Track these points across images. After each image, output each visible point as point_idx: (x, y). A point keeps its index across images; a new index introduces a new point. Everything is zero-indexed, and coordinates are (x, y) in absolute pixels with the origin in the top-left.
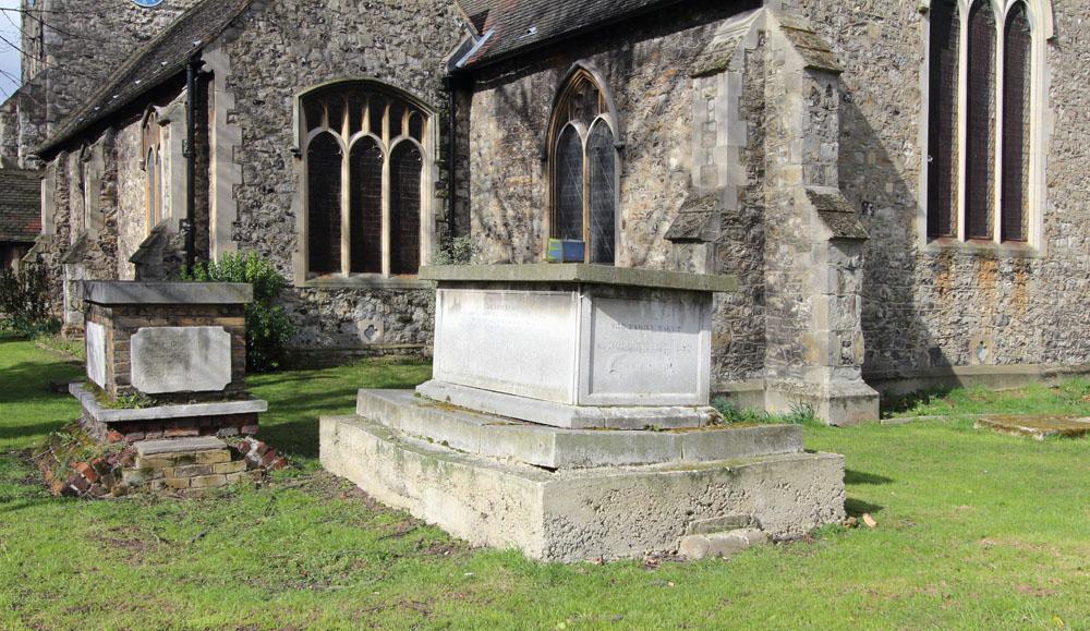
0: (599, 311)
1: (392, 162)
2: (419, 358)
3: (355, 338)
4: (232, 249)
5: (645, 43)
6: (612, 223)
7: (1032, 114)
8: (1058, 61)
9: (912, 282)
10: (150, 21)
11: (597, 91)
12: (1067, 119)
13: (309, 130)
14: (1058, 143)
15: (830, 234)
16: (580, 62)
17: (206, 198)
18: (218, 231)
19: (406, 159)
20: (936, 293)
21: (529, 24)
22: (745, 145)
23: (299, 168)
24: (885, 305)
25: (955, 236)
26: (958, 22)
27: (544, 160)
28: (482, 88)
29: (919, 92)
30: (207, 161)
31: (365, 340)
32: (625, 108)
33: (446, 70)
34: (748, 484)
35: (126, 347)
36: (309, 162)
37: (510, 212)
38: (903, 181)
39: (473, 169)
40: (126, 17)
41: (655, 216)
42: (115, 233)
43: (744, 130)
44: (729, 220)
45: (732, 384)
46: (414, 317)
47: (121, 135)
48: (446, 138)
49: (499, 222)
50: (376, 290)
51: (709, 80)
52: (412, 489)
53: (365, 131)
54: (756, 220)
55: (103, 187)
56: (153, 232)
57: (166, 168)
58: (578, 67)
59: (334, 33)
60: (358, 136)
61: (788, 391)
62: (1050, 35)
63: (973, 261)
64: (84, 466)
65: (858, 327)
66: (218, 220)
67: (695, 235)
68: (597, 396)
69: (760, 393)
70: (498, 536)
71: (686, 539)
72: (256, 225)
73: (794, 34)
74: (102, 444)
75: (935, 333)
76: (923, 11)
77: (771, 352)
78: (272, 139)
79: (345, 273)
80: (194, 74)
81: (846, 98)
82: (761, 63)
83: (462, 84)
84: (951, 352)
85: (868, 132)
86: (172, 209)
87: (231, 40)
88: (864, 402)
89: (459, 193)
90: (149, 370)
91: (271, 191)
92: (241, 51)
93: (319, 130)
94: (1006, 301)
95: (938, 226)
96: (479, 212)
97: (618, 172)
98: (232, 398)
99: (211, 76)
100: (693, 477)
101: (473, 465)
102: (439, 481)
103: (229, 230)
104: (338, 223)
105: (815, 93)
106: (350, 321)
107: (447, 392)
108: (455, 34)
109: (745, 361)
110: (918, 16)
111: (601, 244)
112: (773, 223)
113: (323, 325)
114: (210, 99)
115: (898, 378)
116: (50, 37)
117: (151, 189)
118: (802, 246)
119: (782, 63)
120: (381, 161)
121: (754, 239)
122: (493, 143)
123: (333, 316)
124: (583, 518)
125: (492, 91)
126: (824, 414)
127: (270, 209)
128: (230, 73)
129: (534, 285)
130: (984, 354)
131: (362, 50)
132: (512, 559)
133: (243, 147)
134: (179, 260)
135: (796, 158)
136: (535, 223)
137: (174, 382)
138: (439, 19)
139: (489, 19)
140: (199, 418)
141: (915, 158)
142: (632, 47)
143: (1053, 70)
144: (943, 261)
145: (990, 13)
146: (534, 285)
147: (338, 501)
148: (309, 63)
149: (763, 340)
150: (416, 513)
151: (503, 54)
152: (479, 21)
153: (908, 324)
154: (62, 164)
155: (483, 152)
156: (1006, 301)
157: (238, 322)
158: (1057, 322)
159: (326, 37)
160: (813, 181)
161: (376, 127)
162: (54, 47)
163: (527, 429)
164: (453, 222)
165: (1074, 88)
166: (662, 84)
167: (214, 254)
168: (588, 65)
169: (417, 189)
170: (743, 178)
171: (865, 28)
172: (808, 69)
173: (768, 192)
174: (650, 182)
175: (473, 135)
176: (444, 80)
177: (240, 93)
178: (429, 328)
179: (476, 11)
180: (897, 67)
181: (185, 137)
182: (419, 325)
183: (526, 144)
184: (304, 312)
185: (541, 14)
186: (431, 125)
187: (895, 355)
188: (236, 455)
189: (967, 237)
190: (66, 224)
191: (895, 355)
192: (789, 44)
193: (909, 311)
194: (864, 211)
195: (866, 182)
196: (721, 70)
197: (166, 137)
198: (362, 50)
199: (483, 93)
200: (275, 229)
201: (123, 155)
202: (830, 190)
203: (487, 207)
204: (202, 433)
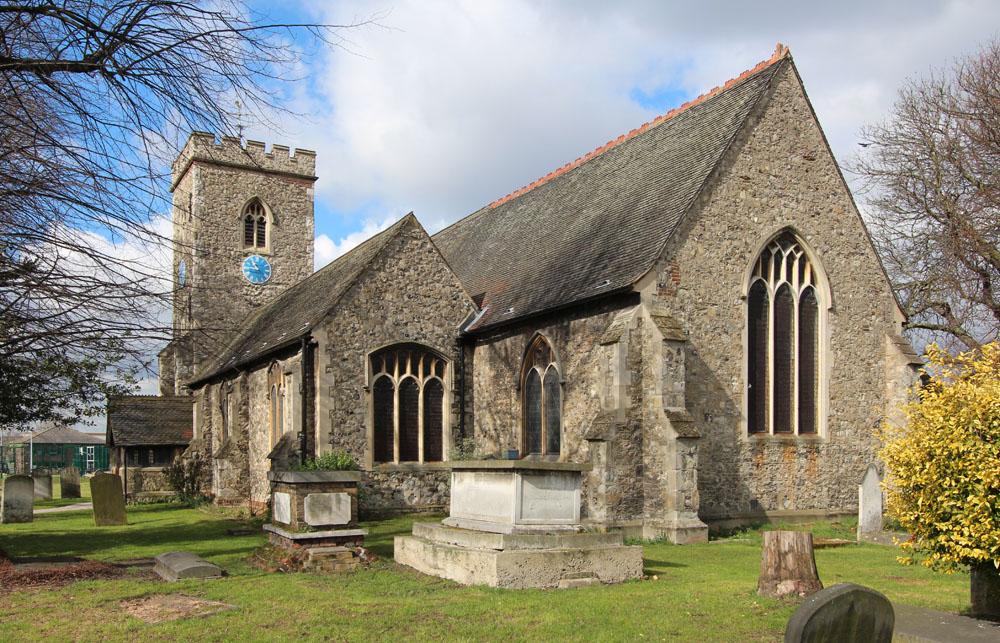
0: (525, 482)
1: (425, 392)
2: (440, 512)
3: (402, 502)
4: (329, 449)
5: (576, 321)
6: (559, 428)
7: (820, 356)
8: (836, 321)
9: (738, 461)
10: (260, 293)
11: (550, 348)
12: (843, 357)
13: (374, 374)
14: (837, 373)
15: (677, 435)
16: (539, 331)
17: (313, 418)
18: (321, 437)
19: (434, 390)
20: (755, 468)
21: (510, 305)
22: (630, 383)
23: (369, 398)
24: (721, 474)
25: (768, 432)
26: (768, 302)
27: (518, 390)
28: (481, 344)
29: (741, 347)
30: (314, 396)
31: (409, 503)
32: (565, 359)
33: (458, 333)
34: (591, 558)
35: (302, 503)
36: (374, 394)
37: (498, 422)
38: (731, 400)
39: (475, 395)
40: (245, 292)
41: (583, 424)
42: (247, 438)
43: (630, 376)
44: (620, 428)
45: (623, 522)
46: (439, 488)
47: (251, 376)
48: (459, 376)
49: (492, 428)
50: (415, 472)
51: (609, 347)
52: (440, 566)
53: (408, 373)
54: (637, 427)
55: (240, 410)
56: (281, 440)
57: (289, 401)
58: (538, 334)
59: (389, 314)
60: (404, 377)
61: (655, 525)
62: (830, 307)
63: (779, 447)
64: (286, 560)
65: (696, 487)
66: (321, 432)
67: (600, 437)
68: (524, 520)
69: (640, 528)
70: (478, 580)
71: (561, 581)
72: (342, 434)
73: (658, 319)
74: (292, 550)
75: (754, 491)
76: (743, 298)
77: (647, 503)
78: (352, 381)
79: (396, 462)
80: (306, 344)
81: (693, 353)
82: (640, 336)
83: (468, 342)
84: (765, 502)
85: (708, 372)
86: (290, 424)
87: (329, 323)
88: (699, 531)
89: (467, 410)
90: (314, 514)
91: (352, 413)
92: (334, 329)
93: (380, 375)
94: (803, 470)
95: (756, 424)
96: (479, 421)
97: (561, 398)
98: (351, 528)
99: (316, 345)
100: (565, 554)
101: (466, 551)
102: (453, 559)
103: (327, 437)
104: (392, 431)
105: (670, 353)
106: (399, 491)
107: (457, 522)
108: (464, 310)
109: (631, 509)
110: (740, 301)
111: (552, 441)
112: (647, 428)
113: (383, 494)
114: (315, 359)
115: (729, 518)
116: (197, 308)
117: (274, 412)
118: (662, 442)
119: (651, 336)
120: (418, 392)
121: (636, 438)
122: (487, 378)
123: (389, 488)
124: (514, 570)
125: (487, 346)
126: (673, 538)
127: (351, 423)
128: (327, 343)
129: (497, 470)
130: (787, 503)
131: (406, 324)
132: (485, 588)
133: (336, 387)
134: (297, 456)
135: (659, 391)
136: (514, 428)
137: (325, 520)
138: (454, 302)
139: (486, 300)
140: (336, 537)
141: (740, 386)
142: (569, 323)
143: (833, 327)
144: (759, 448)
145: (789, 295)
146: (497, 470)
147: (405, 573)
148: (374, 334)
149: (643, 496)
150: (442, 576)
151: (492, 325)
152: (478, 300)
153: (736, 486)
154: (208, 392)
155: (482, 384)
156: (803, 470)
157: (354, 490)
158: (839, 483)
159: (384, 318)
160: (669, 405)
161: (415, 371)
162: (199, 315)
163: (491, 535)
164: (463, 429)
165: (848, 337)
166: (586, 346)
167: (318, 453)
168: (544, 333)
169: (441, 409)
170: (629, 403)
171: (705, 311)
172: (665, 340)
173: (645, 411)
174: (580, 404)
175: (475, 373)
176: (457, 340)
177: (333, 354)
178: (447, 495)
179: (477, 293)
180: (727, 333)
181: (301, 382)
182: (442, 493)
183: (508, 380)
184: (371, 486)
185: (517, 299)
186: (449, 369)
187: (727, 504)
188: (355, 555)
189: (776, 431)
190: (209, 431)
191: (727, 504)
192: (654, 325)
193: (736, 478)
194: (706, 419)
195: (707, 402)
196: (616, 342)
197: (289, 382)
198: (406, 324)
199: (481, 347)
200: (354, 436)
201: (253, 389)
202: (680, 409)
203: (484, 419)
204: (338, 545)
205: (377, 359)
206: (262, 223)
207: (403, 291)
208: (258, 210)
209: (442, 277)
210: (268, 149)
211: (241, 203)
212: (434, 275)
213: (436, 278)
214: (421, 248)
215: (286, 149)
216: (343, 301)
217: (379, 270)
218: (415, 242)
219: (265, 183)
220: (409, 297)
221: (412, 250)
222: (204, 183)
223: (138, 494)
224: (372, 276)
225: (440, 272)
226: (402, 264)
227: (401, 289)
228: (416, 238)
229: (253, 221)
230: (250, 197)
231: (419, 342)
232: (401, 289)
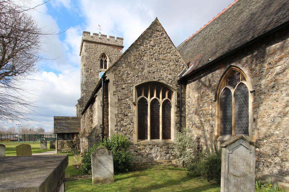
3: (152, 159)
13: (138, 97)
17: (108, 118)
19: (167, 105)
33: (179, 78)
36: (138, 107)
53: (155, 97)
55: (89, 119)
83: (184, 81)
87: (115, 70)
89: (182, 115)
91: (127, 115)
92: (118, 73)
93: (141, 97)
108: (181, 67)
128: (114, 80)
131: (154, 73)
138: (177, 63)
159: (143, 69)
161: (158, 96)
177: (117, 86)
184: (137, 152)
198: (154, 73)
205: (139, 88)
206: (106, 61)
207: (152, 57)
208: (105, 57)
209: (171, 51)
210: (108, 37)
211: (99, 54)
212: (167, 49)
213: (168, 51)
214: (161, 36)
215: (114, 37)
216: (122, 59)
217: (140, 45)
218: (158, 33)
219: (107, 48)
220: (155, 59)
221: (157, 37)
222: (87, 48)
223: (62, 149)
224: (137, 48)
225: (170, 48)
226: (152, 43)
227: (151, 55)
228: (158, 31)
229: (103, 61)
230: (102, 53)
231: (160, 81)
232: (151, 55)
